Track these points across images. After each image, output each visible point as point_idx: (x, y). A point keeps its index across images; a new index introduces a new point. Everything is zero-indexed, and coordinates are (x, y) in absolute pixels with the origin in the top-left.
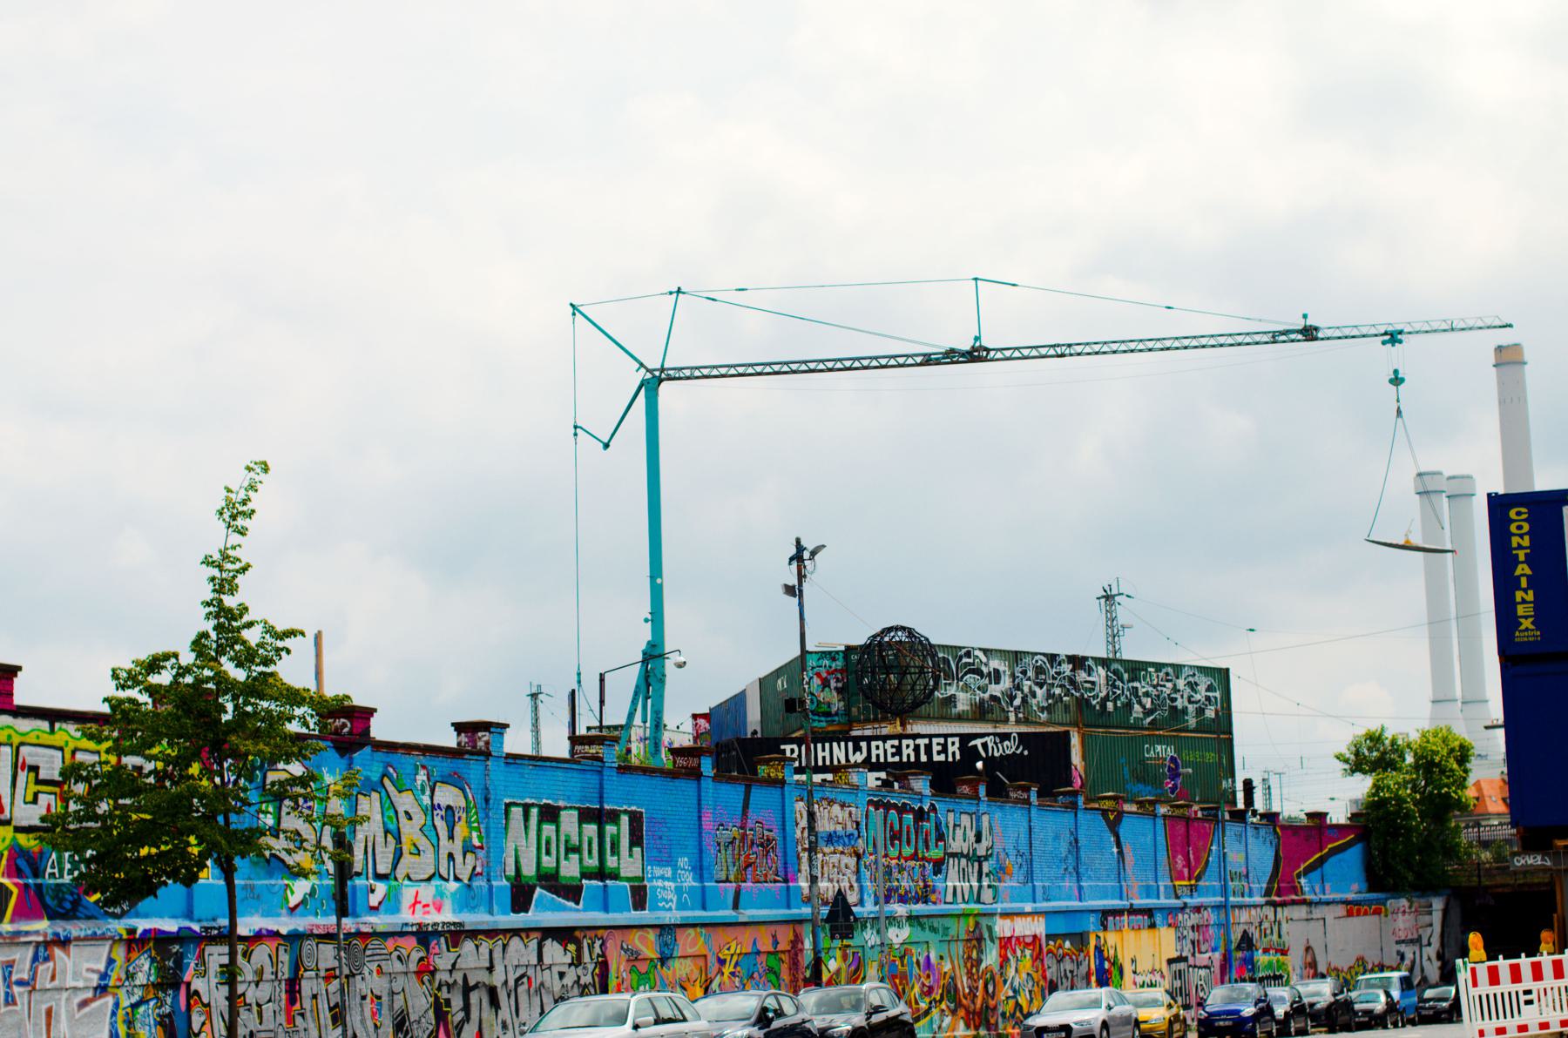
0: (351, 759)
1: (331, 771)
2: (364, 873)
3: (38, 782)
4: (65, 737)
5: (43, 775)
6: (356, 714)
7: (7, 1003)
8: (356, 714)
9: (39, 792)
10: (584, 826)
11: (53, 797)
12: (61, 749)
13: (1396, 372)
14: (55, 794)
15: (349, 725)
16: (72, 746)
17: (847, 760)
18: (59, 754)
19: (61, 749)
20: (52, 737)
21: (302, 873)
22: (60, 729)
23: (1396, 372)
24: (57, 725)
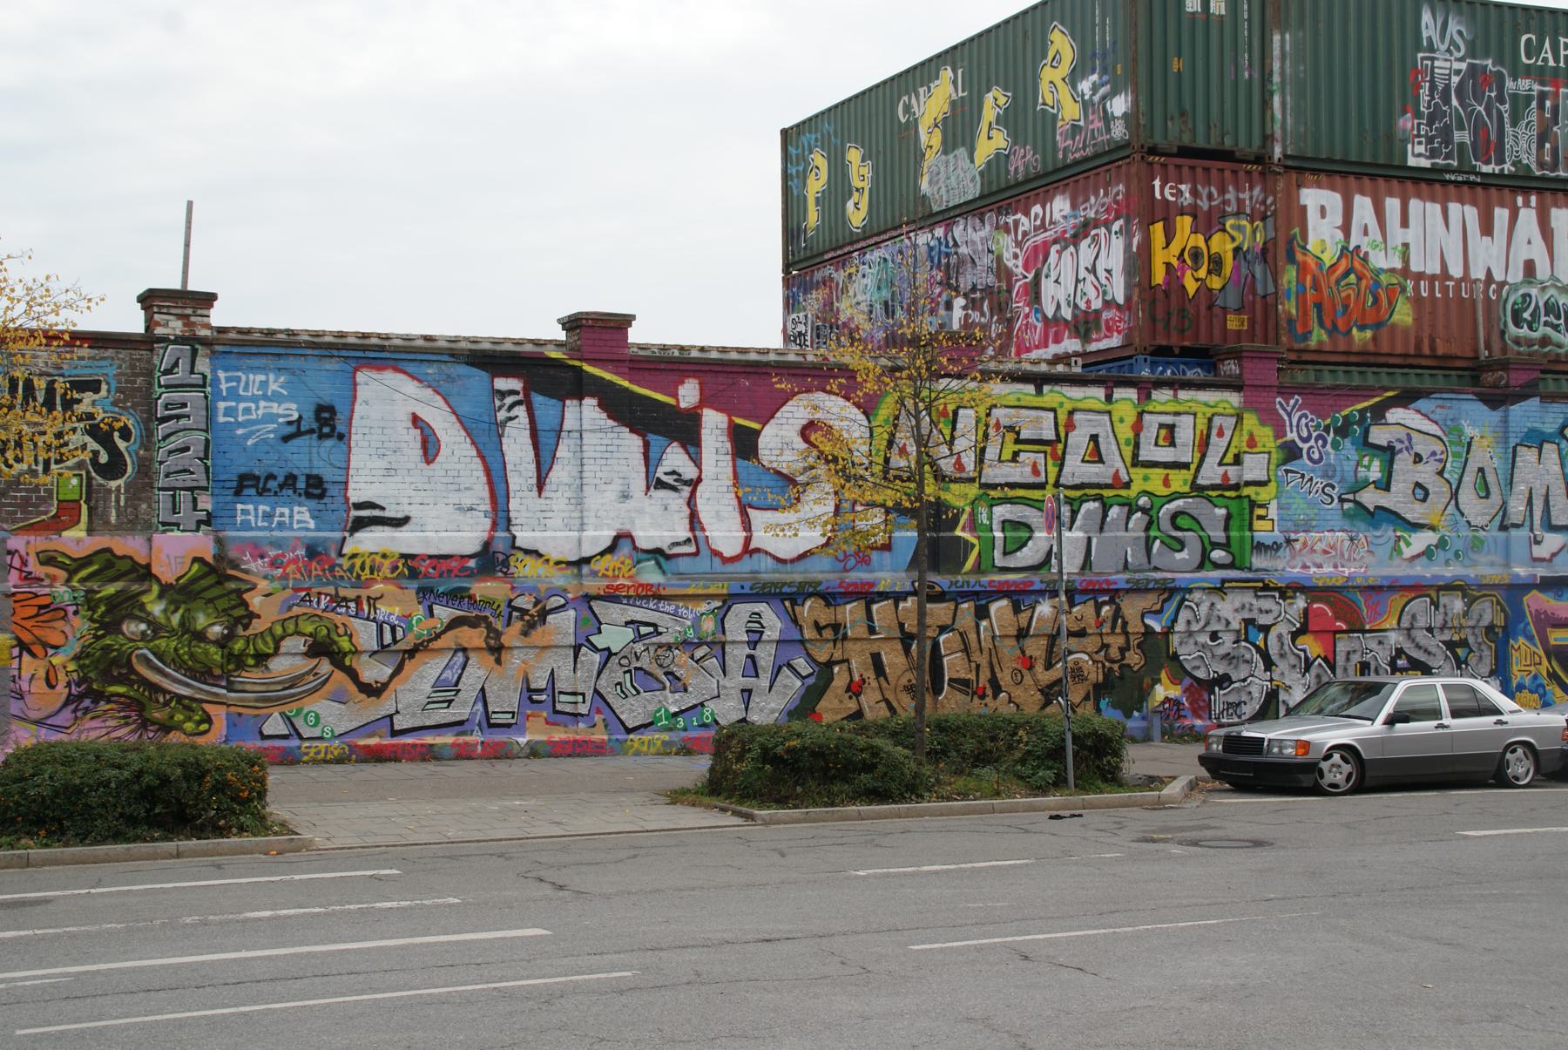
0: (1506, 411)
1: (1473, 424)
2: (1527, 523)
3: (1018, 441)
4: (1059, 398)
5: (1024, 435)
6: (1245, 354)
7: (750, 691)
8: (1245, 354)
9: (1020, 451)
10: (1554, 212)
11: (1042, 455)
12: (1054, 410)
13: (498, 661)
14: (1045, 452)
15: (241, 393)
16: (1068, 406)
17: (194, 353)
18: (1051, 415)
19: (1054, 410)
20: (1040, 399)
21: (1416, 527)
22: (1051, 391)
23: (498, 661)
24: (1046, 388)
